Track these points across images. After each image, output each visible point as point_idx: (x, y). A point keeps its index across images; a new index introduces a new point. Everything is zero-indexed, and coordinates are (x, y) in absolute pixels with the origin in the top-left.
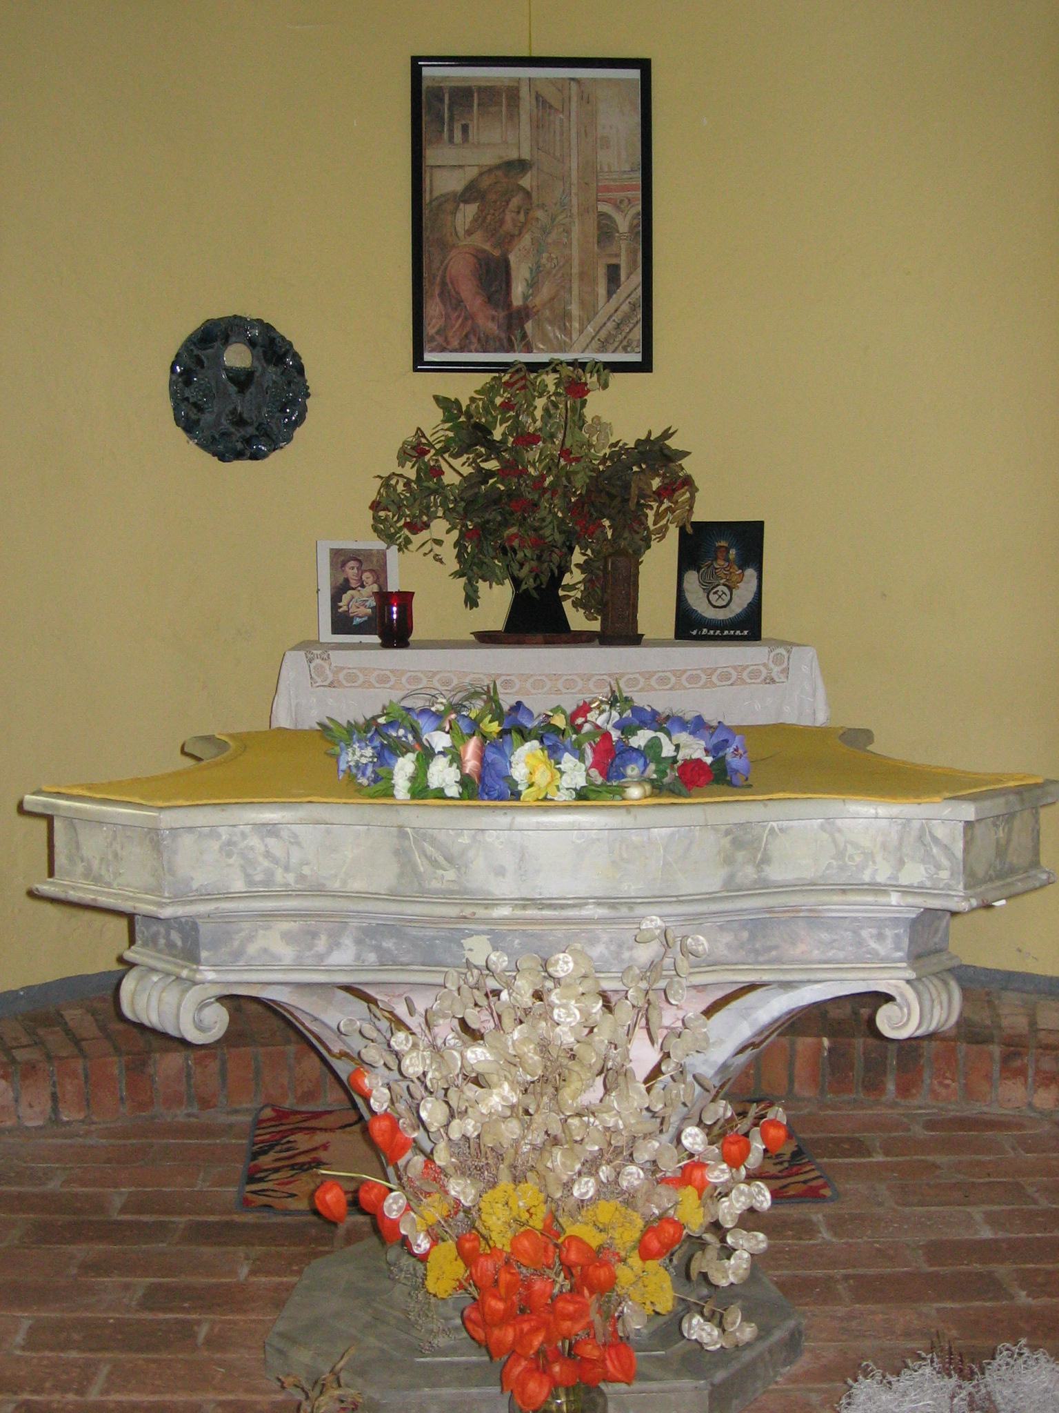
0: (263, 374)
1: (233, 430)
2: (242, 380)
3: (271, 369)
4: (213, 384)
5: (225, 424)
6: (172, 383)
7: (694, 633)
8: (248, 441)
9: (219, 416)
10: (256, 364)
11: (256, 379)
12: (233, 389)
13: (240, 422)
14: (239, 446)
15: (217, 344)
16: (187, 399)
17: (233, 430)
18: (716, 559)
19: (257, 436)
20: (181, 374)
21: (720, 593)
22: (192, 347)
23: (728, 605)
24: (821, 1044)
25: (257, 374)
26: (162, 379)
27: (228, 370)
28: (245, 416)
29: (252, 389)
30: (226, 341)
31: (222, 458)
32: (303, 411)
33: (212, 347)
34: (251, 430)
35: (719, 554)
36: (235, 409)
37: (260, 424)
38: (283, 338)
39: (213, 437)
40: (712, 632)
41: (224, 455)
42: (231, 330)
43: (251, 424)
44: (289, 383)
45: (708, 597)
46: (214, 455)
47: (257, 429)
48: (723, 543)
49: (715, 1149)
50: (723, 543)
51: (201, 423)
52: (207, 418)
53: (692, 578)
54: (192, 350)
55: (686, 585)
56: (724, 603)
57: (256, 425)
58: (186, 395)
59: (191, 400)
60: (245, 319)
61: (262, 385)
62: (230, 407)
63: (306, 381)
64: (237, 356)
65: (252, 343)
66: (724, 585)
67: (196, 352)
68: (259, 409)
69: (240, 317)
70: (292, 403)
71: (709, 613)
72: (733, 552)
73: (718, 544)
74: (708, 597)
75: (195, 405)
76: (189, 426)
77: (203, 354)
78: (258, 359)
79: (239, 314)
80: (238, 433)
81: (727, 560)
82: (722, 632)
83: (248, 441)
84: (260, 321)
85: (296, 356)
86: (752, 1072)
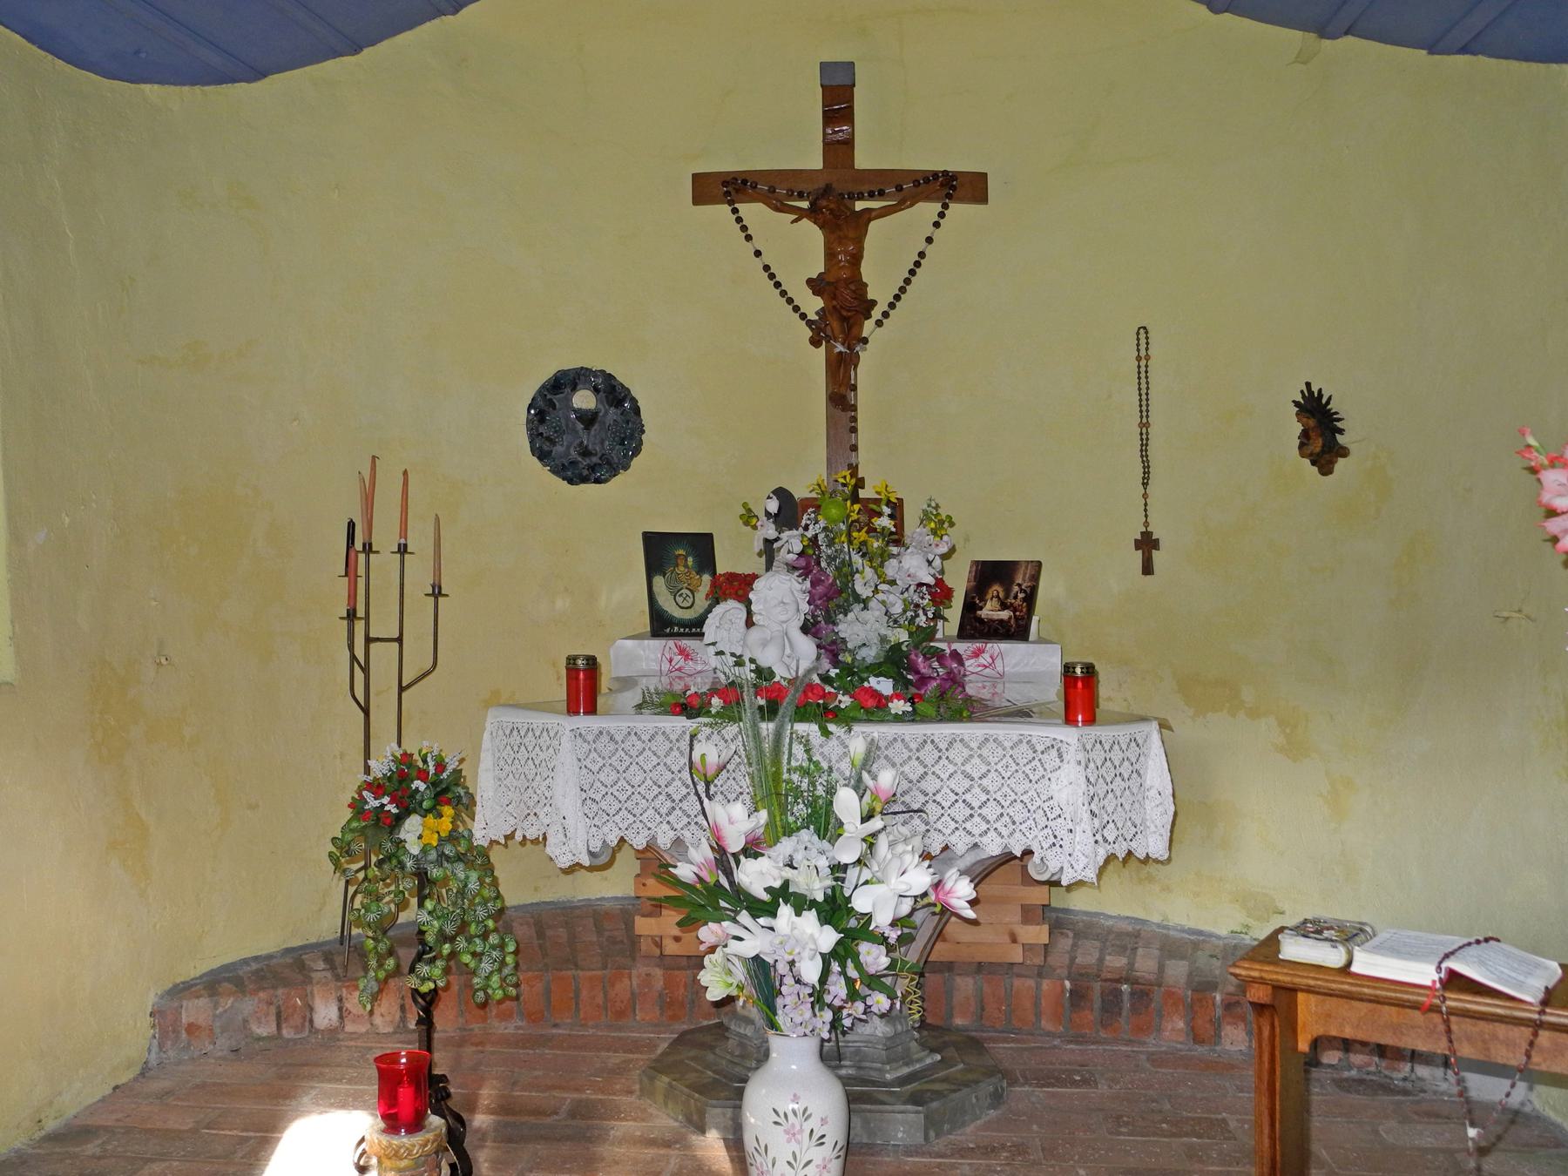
0: (606, 412)
1: (580, 459)
2: (589, 419)
3: (613, 409)
4: (563, 421)
5: (574, 454)
6: (529, 421)
7: (668, 630)
8: (593, 468)
9: (568, 447)
10: (600, 406)
11: (599, 418)
12: (580, 426)
13: (586, 453)
14: (585, 472)
15: (568, 390)
16: (541, 434)
17: (580, 459)
18: (677, 565)
19: (600, 464)
20: (536, 415)
21: (684, 596)
22: (546, 393)
23: (690, 607)
24: (1063, 986)
25: (601, 414)
26: (522, 415)
27: (576, 411)
28: (590, 447)
29: (596, 426)
30: (574, 389)
31: (571, 482)
32: (641, 443)
33: (562, 393)
34: (595, 460)
35: (679, 561)
36: (582, 442)
37: (603, 455)
38: (623, 386)
39: (563, 465)
40: (682, 630)
41: (572, 480)
42: (579, 379)
43: (596, 455)
44: (628, 422)
45: (675, 599)
46: (564, 479)
47: (600, 459)
48: (681, 552)
49: (493, 1134)
50: (681, 552)
51: (553, 454)
52: (558, 449)
53: (659, 581)
54: (546, 395)
55: (655, 589)
56: (689, 605)
57: (599, 455)
58: (540, 431)
59: (545, 435)
60: (590, 370)
61: (604, 423)
62: (578, 441)
63: (642, 420)
64: (584, 400)
65: (596, 390)
66: (687, 588)
67: (549, 397)
68: (602, 443)
69: (587, 369)
70: (632, 437)
71: (677, 613)
72: (690, 560)
73: (677, 553)
74: (675, 599)
75: (548, 439)
76: (542, 455)
77: (556, 399)
78: (602, 403)
79: (585, 366)
80: (586, 462)
81: (686, 566)
82: (690, 630)
83: (593, 468)
84: (603, 372)
85: (634, 401)
86: (1004, 1008)
